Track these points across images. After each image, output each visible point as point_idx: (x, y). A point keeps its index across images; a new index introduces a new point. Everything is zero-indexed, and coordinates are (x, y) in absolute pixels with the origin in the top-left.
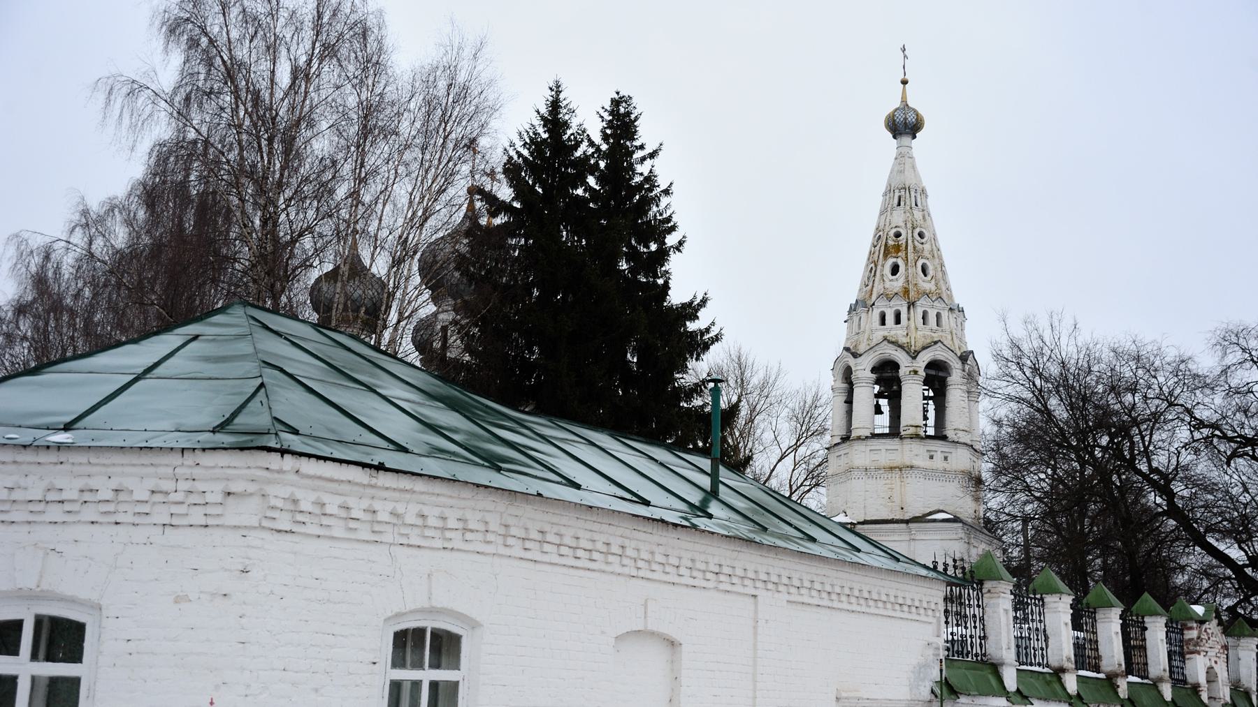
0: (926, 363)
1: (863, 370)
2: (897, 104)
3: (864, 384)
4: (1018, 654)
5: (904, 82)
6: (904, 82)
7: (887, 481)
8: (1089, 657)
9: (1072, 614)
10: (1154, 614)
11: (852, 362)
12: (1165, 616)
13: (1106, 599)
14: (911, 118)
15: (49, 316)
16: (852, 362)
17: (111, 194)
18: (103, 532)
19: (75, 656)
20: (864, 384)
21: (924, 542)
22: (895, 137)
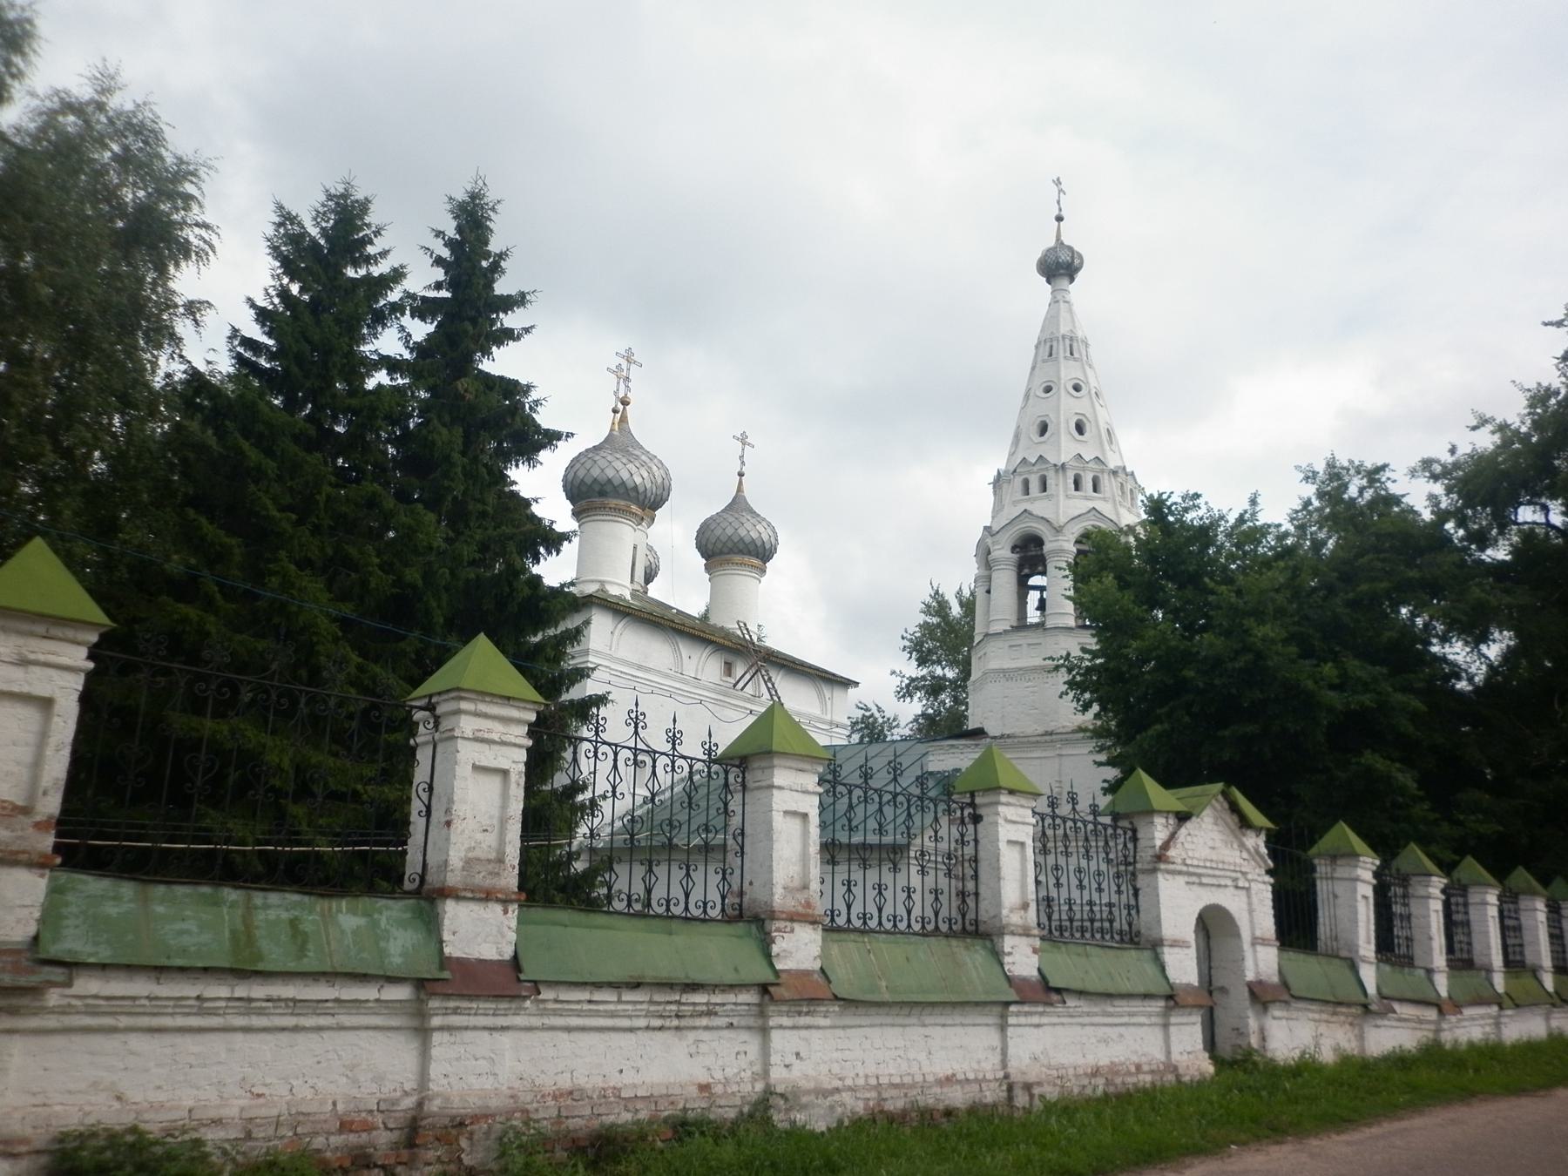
0: (1076, 535)
1: (1003, 552)
2: (1052, 243)
3: (1002, 567)
4: (303, 1114)
5: (1059, 219)
6: (1059, 219)
7: (1030, 684)
8: (1398, 937)
9: (1273, 886)
10: (1533, 893)
11: (989, 541)
12: (1542, 895)
13: (1434, 848)
14: (1064, 257)
15: (539, 647)
16: (989, 541)
17: (168, 133)
18: (751, 883)
19: (272, 733)
20: (1002, 567)
21: (1072, 758)
22: (1049, 282)
